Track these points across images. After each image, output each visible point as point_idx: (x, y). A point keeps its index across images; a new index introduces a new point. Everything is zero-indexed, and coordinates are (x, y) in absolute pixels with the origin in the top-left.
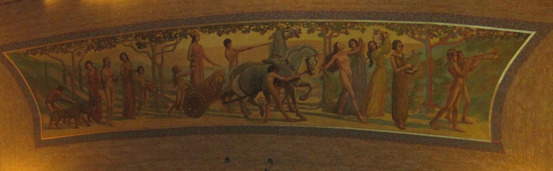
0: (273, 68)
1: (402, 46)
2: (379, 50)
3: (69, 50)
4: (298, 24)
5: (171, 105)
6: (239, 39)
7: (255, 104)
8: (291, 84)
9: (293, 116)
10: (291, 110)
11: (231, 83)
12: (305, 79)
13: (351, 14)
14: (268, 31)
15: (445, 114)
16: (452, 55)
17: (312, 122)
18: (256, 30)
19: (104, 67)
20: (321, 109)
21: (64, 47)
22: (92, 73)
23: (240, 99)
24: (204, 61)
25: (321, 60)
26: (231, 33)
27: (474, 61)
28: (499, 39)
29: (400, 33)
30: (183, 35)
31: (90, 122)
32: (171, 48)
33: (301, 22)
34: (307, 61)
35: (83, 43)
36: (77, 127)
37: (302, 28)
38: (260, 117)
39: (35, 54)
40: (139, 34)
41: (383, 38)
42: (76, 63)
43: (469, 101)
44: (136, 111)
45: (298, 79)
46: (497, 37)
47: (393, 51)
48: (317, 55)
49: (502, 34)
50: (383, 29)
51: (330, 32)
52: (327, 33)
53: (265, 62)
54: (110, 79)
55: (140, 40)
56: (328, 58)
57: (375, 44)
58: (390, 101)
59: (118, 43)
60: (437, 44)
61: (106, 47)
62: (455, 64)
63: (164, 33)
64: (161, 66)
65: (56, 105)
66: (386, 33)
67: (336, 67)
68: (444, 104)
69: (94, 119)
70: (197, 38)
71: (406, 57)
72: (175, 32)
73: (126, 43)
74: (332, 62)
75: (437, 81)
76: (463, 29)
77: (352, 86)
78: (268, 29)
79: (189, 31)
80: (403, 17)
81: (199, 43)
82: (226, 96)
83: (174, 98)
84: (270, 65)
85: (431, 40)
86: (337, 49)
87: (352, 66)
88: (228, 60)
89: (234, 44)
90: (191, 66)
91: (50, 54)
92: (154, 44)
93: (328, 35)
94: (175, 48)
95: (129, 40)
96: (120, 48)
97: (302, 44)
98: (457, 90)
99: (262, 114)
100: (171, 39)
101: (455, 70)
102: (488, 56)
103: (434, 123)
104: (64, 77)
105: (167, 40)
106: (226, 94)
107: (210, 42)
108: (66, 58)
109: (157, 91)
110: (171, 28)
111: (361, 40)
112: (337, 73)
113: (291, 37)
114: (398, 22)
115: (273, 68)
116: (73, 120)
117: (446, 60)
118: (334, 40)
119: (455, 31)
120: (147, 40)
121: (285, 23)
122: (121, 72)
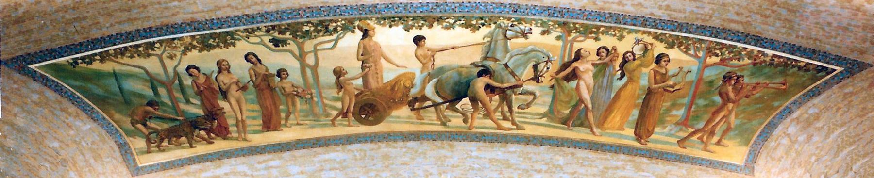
0: (485, 72)
1: (669, 61)
2: (636, 62)
3: (150, 52)
4: (530, 22)
5: (335, 113)
6: (436, 36)
7: (457, 111)
8: (509, 92)
9: (507, 124)
10: (505, 118)
11: (424, 88)
12: (530, 86)
13: (608, 15)
14: (483, 29)
15: (699, 135)
16: (730, 78)
17: (529, 130)
18: (467, 25)
19: (220, 72)
20: (545, 119)
21: (141, 49)
22: (202, 80)
23: (435, 105)
24: (383, 61)
25: (554, 67)
26: (425, 28)
27: (754, 88)
28: (796, 69)
29: (671, 46)
30: (348, 27)
31: (213, 138)
32: (330, 45)
33: (533, 20)
34: (535, 67)
35: (176, 41)
36: (191, 147)
37: (533, 27)
38: (463, 124)
39: (91, 63)
40: (274, 27)
41: (646, 50)
42: (170, 70)
43: (732, 126)
44: (283, 122)
45: (521, 86)
46: (794, 66)
47: (654, 65)
48: (550, 61)
49: (802, 64)
50: (648, 39)
51: (573, 35)
52: (569, 36)
53: (475, 65)
54: (234, 88)
55: (276, 35)
56: (565, 66)
57: (634, 55)
58: (636, 117)
59: (239, 40)
60: (715, 64)
61: (218, 46)
62: (730, 88)
63: (316, 26)
64: (315, 68)
65: (152, 124)
66: (651, 44)
67: (574, 75)
68: (701, 125)
69: (216, 135)
70: (370, 32)
71: (670, 73)
72: (334, 24)
73: (253, 39)
74: (569, 70)
75: (701, 102)
76: (755, 53)
77: (592, 98)
78: (483, 25)
79: (357, 23)
80: (680, 27)
81: (374, 39)
82: (417, 103)
83: (339, 105)
84: (481, 69)
85: (708, 59)
86: (578, 56)
87: (595, 76)
88: (421, 62)
89: (429, 43)
90: (363, 68)
91: (119, 60)
92: (301, 41)
93: (569, 38)
94: (335, 45)
95: (256, 36)
96: (243, 46)
97: (530, 47)
98: (722, 114)
99: (465, 121)
100: (327, 31)
101: (727, 94)
102: (774, 86)
103: (681, 142)
104: (154, 88)
105: (321, 34)
106: (416, 99)
107: (393, 40)
108: (152, 65)
109: (312, 98)
110: (327, 18)
111: (614, 49)
112: (573, 84)
113: (517, 37)
114: (672, 33)
115: (485, 72)
116: (183, 139)
117: (721, 82)
118: (577, 46)
119: (744, 53)
120: (288, 35)
121: (509, 19)
122: (251, 77)
